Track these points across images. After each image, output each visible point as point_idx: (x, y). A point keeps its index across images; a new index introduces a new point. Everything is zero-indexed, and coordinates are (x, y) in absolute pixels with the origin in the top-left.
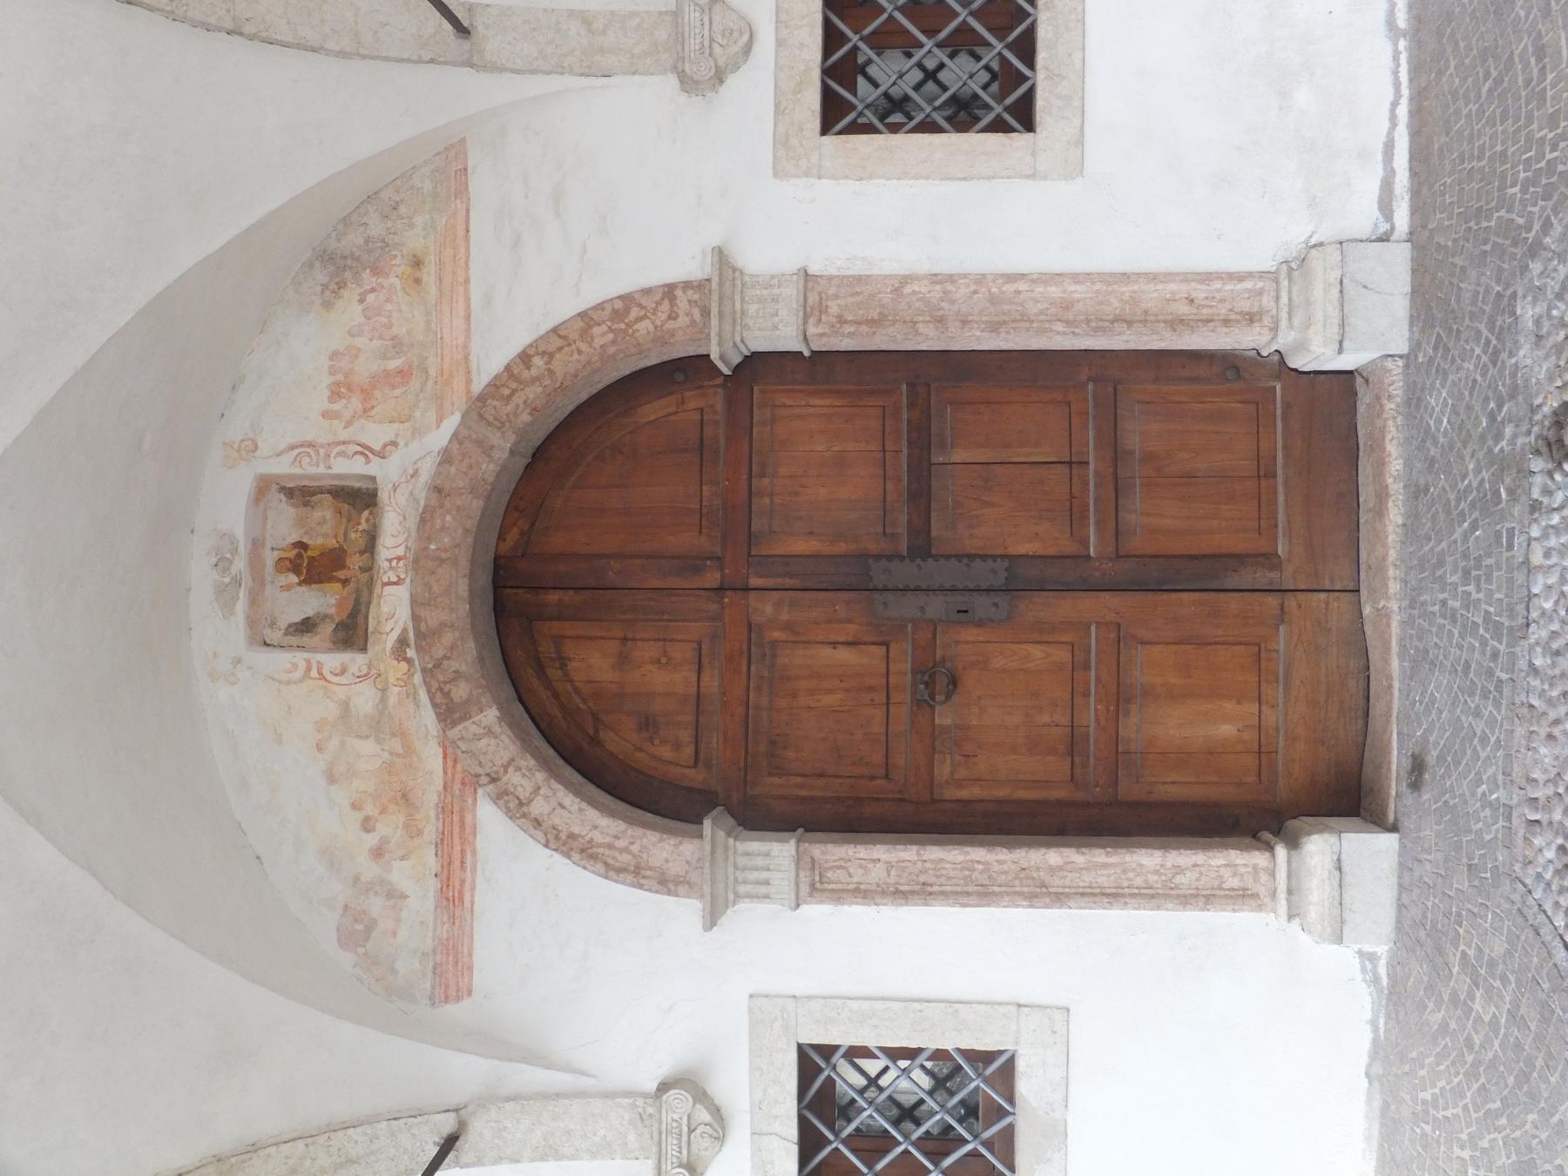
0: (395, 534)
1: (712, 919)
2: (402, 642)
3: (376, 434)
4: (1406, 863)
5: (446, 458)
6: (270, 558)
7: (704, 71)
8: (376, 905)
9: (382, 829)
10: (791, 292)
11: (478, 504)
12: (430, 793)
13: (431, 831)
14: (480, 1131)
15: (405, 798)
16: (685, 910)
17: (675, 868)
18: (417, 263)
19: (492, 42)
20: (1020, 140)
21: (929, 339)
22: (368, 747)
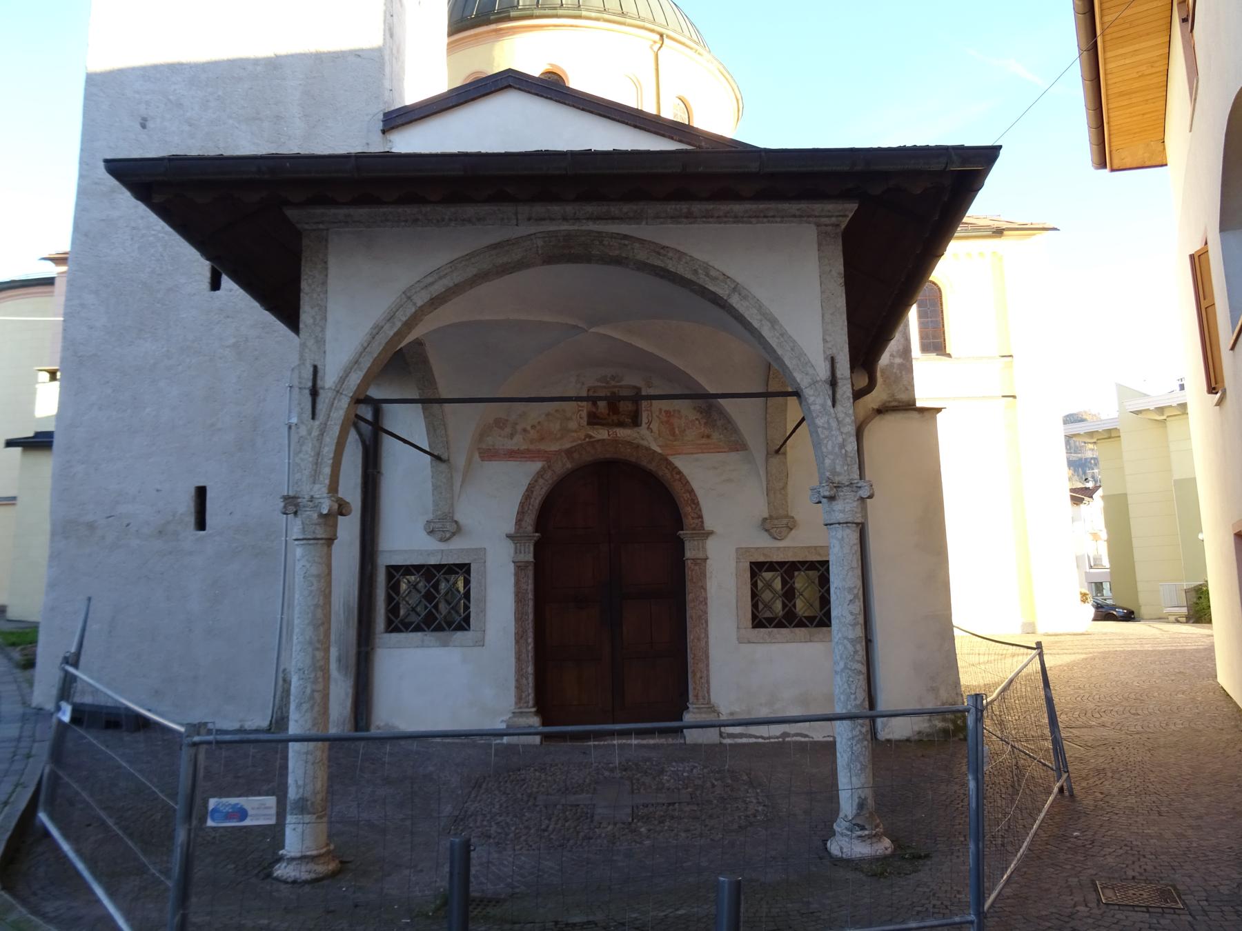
0: (623, 433)
1: (509, 536)
2: (591, 437)
3: (654, 426)
4: (535, 746)
5: (648, 449)
6: (616, 390)
7: (768, 526)
8: (508, 430)
9: (532, 432)
10: (701, 555)
11: (633, 460)
12: (543, 447)
13: (532, 447)
14: (443, 466)
15: (542, 439)
16: (510, 528)
17: (523, 524)
18: (708, 437)
19: (775, 460)
20: (749, 624)
21: (689, 597)
22: (558, 426)
